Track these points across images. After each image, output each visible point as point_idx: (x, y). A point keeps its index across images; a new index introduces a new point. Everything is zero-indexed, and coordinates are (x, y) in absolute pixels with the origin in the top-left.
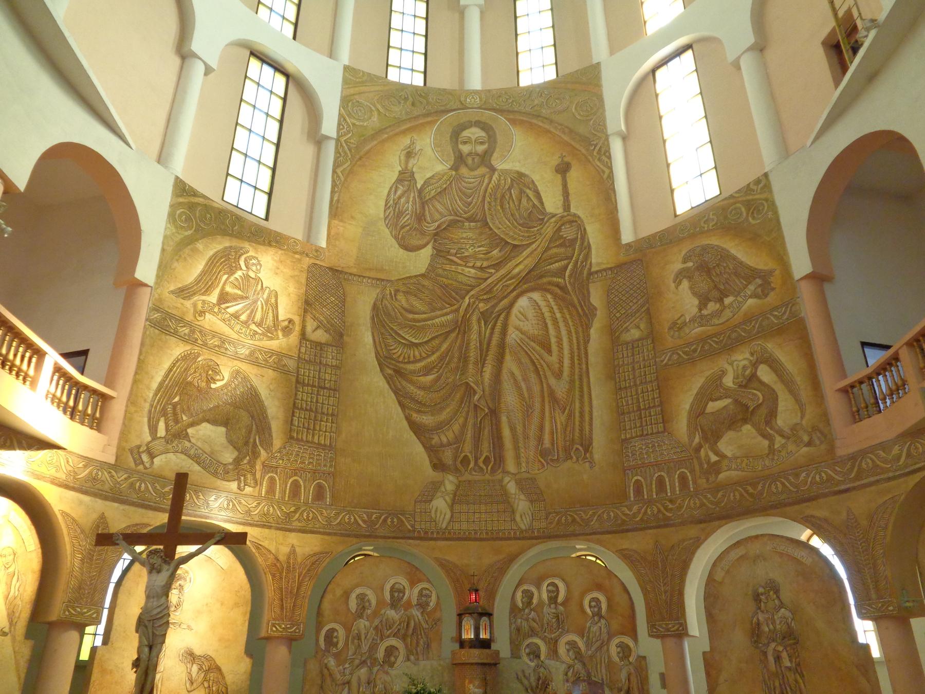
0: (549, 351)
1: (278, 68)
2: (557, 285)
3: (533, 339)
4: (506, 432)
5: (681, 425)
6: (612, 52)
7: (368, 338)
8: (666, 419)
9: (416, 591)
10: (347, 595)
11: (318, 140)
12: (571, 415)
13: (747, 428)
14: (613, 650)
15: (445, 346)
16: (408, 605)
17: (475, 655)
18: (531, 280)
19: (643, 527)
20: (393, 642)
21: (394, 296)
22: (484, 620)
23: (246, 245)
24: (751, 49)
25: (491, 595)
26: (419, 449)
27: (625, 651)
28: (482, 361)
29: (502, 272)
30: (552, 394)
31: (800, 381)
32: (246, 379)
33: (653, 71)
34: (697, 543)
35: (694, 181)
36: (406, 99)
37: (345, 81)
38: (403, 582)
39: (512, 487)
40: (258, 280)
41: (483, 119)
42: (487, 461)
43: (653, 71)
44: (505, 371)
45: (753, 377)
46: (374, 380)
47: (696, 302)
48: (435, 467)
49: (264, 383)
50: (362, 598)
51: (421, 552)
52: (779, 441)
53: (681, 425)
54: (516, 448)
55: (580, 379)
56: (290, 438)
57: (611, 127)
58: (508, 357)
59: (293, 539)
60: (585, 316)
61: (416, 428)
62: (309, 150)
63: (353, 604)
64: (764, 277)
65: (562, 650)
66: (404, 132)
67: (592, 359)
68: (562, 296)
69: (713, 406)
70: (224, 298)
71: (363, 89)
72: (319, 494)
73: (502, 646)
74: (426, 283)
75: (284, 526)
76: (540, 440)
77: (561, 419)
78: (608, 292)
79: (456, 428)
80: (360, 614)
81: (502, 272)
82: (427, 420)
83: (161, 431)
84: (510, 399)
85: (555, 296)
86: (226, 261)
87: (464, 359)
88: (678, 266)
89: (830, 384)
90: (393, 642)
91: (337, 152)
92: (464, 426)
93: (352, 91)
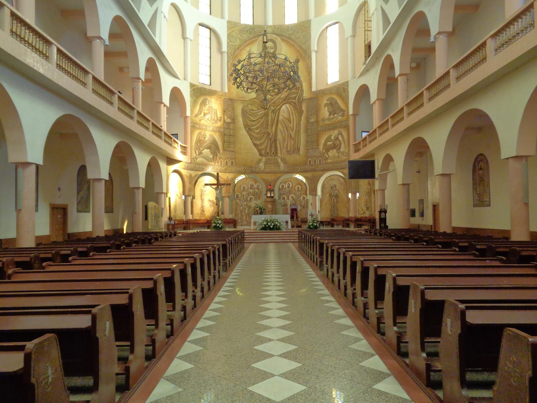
0: (290, 123)
1: (207, 27)
2: (293, 102)
3: (286, 119)
4: (278, 146)
5: (321, 147)
6: (316, 16)
7: (241, 120)
8: (318, 145)
9: (256, 185)
10: (240, 186)
11: (222, 53)
12: (295, 142)
13: (335, 150)
14: (301, 198)
15: (262, 121)
16: (254, 188)
17: (270, 199)
18: (286, 100)
19: (310, 171)
20: (251, 196)
21: (247, 106)
22: (272, 192)
23: (208, 97)
24: (351, 36)
25: (274, 186)
26: (256, 150)
27: (304, 198)
28: (272, 125)
29: (278, 97)
30: (290, 135)
31: (346, 140)
32: (212, 136)
33: (327, 27)
34: (321, 176)
35: (333, 76)
36: (247, 31)
37: (229, 28)
38: (253, 183)
39: (279, 160)
40: (212, 107)
41: (273, 38)
42: (273, 153)
43: (327, 27)
44: (278, 128)
45: (338, 138)
46: (243, 132)
47: (328, 114)
48: (260, 155)
49: (217, 138)
50: (244, 187)
51: (258, 177)
52: (340, 154)
53: (321, 147)
54: (281, 150)
55: (298, 132)
56: (224, 150)
57: (312, 49)
58: (279, 124)
59: (227, 174)
60: (300, 113)
61: (255, 145)
62: (219, 56)
63: (242, 188)
64: (344, 111)
65: (290, 198)
66: (247, 45)
67: (302, 126)
68: (294, 105)
69: (329, 143)
70: (205, 115)
71: (234, 29)
72: (232, 164)
73: (276, 197)
74: (256, 100)
75: (225, 172)
76: (287, 148)
77: (292, 142)
78: (307, 106)
79: (265, 144)
80: (244, 190)
81: (278, 97)
82: (258, 142)
83: (197, 153)
84: (279, 137)
85: (293, 106)
86: (204, 103)
87: (267, 124)
88: (325, 102)
89: (352, 143)
90: (251, 196)
91: (228, 57)
92: (267, 144)
93: (230, 31)
